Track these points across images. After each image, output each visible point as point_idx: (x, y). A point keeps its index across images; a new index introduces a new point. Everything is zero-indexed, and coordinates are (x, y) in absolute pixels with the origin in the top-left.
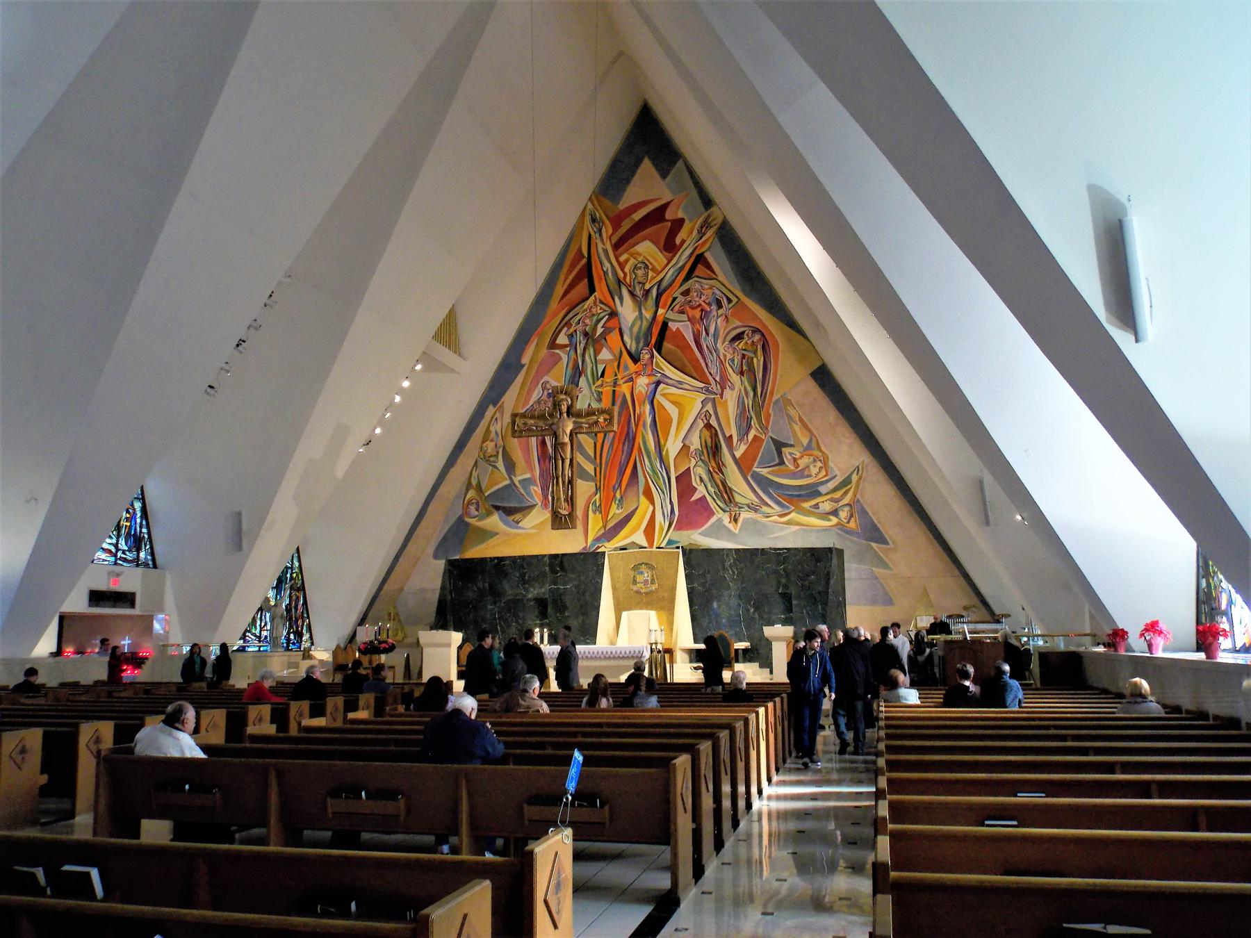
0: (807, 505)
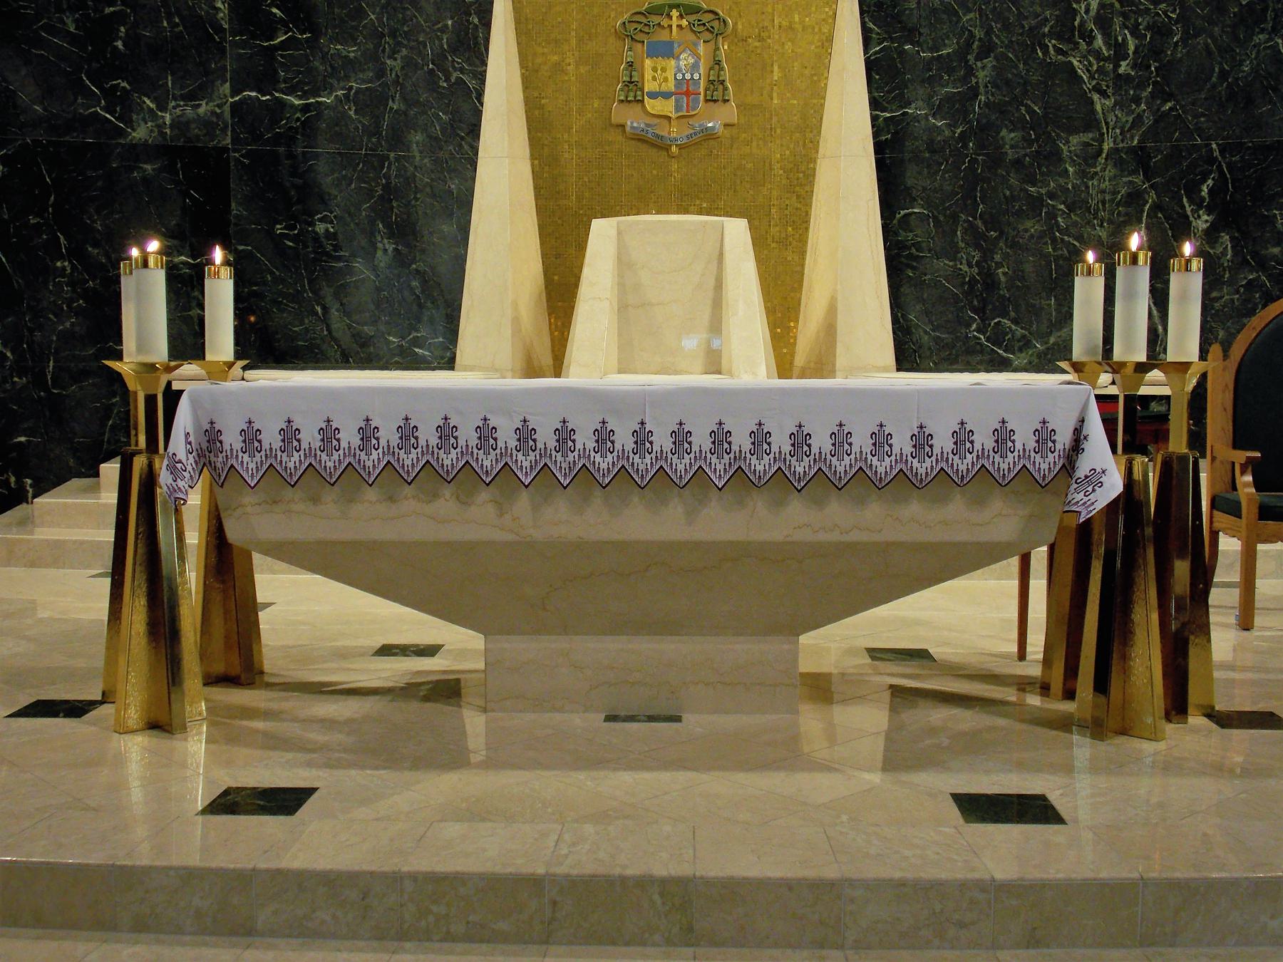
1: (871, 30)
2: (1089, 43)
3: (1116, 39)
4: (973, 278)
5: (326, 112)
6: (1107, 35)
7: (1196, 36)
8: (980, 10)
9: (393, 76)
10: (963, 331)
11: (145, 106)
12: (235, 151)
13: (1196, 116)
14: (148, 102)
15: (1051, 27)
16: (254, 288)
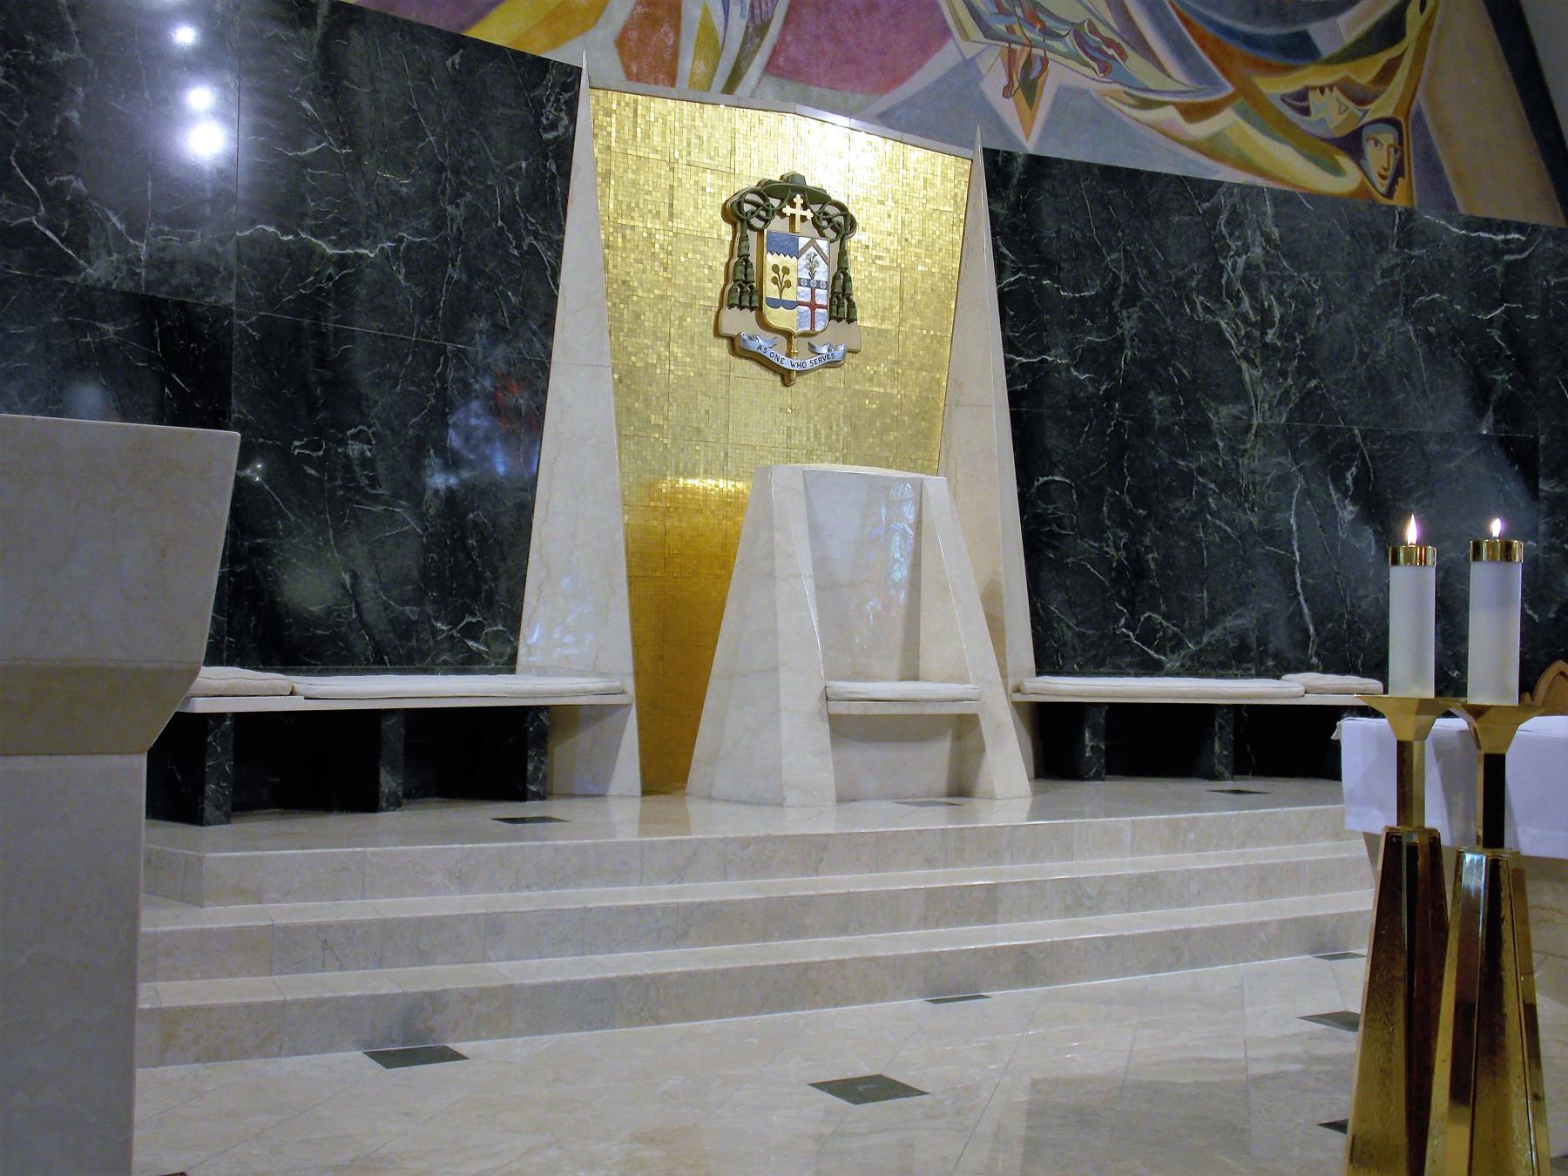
0: (1275, 87)
1: (1005, 257)
2: (1237, 305)
3: (1263, 305)
4: (1120, 563)
5: (368, 271)
6: (1253, 297)
7: (1338, 311)
8: (1125, 250)
9: (454, 229)
10: (1110, 627)
11: (108, 226)
12: (241, 317)
13: (1340, 398)
14: (114, 219)
15: (1199, 281)
16: (259, 541)
